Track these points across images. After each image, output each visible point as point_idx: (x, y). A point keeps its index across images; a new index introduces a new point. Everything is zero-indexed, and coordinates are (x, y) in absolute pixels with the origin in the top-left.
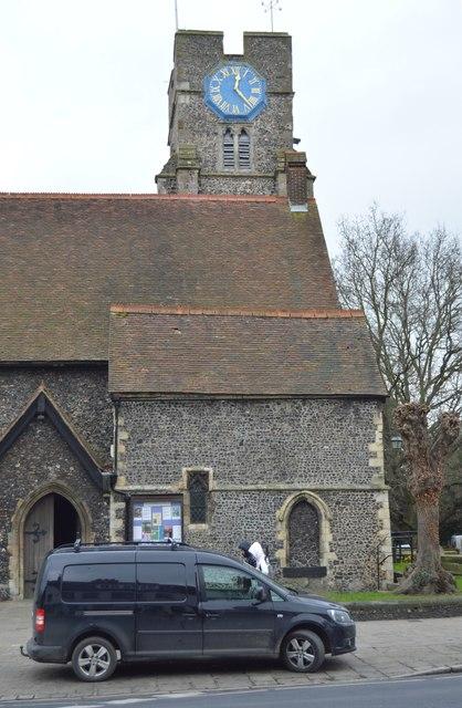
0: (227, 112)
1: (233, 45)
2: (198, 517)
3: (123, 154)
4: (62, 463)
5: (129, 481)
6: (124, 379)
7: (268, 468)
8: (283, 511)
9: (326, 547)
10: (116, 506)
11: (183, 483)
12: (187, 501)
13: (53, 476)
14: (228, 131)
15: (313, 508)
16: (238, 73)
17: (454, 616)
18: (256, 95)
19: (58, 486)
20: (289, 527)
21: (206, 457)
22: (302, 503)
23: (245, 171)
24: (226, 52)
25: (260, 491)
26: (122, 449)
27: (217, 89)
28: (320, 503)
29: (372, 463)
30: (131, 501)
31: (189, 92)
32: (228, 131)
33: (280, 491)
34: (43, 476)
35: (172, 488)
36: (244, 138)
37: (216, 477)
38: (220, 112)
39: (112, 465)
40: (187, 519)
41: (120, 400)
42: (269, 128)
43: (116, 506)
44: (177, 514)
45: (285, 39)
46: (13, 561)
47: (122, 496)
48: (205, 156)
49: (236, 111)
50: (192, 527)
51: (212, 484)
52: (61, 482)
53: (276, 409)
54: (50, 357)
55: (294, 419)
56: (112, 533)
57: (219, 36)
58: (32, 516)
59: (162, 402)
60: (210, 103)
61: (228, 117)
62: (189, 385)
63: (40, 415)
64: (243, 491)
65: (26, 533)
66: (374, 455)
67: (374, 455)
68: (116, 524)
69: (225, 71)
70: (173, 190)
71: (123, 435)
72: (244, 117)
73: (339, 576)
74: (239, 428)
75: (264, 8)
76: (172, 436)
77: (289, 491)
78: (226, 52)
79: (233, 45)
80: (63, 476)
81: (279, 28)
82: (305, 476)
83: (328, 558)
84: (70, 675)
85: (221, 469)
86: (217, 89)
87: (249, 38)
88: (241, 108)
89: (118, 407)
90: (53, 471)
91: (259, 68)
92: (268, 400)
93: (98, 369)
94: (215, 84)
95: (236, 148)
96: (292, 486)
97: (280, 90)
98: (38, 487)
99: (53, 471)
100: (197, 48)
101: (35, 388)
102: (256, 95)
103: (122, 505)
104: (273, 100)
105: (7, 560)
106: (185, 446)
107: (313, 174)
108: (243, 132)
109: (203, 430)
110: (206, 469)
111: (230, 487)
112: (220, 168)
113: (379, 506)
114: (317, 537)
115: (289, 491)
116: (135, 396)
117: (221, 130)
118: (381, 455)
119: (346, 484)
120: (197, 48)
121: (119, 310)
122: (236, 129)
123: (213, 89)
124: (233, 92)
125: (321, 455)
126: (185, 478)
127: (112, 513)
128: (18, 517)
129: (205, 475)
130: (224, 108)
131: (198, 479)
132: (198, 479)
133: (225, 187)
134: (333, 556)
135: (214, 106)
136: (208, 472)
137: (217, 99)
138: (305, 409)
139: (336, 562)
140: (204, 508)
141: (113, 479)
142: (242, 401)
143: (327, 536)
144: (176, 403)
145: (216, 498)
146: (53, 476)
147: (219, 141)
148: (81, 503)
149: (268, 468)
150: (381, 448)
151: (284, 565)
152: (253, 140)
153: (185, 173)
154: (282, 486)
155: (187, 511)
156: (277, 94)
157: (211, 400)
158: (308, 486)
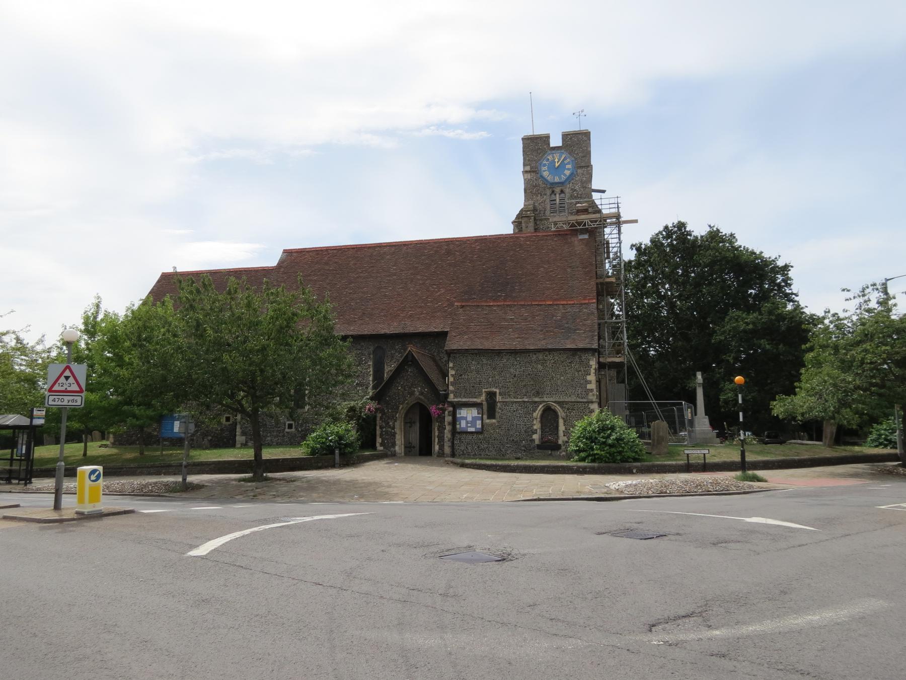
0: (552, 181)
1: (556, 141)
2: (491, 415)
3: (489, 208)
5: (455, 396)
6: (452, 344)
8: (537, 414)
11: (483, 397)
12: (485, 407)
13: (417, 393)
14: (553, 192)
15: (555, 413)
16: (557, 159)
18: (568, 169)
20: (541, 422)
24: (552, 145)
26: (451, 379)
27: (546, 168)
28: (558, 408)
29: (589, 387)
30: (456, 406)
32: (553, 192)
33: (536, 402)
34: (412, 393)
35: (478, 400)
36: (562, 195)
39: (447, 390)
40: (485, 417)
41: (450, 353)
46: (398, 437)
48: (539, 207)
49: (557, 180)
50: (488, 421)
51: (499, 398)
56: (446, 423)
60: (542, 176)
61: (553, 185)
63: (409, 361)
64: (516, 402)
65: (406, 423)
66: (590, 382)
67: (590, 382)
68: (448, 419)
69: (550, 157)
71: (452, 372)
72: (562, 183)
76: (478, 372)
77: (541, 403)
78: (552, 145)
79: (556, 141)
80: (421, 393)
82: (550, 394)
86: (546, 168)
87: (566, 136)
88: (560, 178)
89: (449, 356)
91: (571, 153)
94: (545, 165)
98: (411, 401)
100: (535, 147)
102: (568, 169)
103: (451, 409)
104: (579, 171)
105: (394, 436)
108: (562, 192)
109: (494, 369)
113: (381, 445)
115: (541, 403)
116: (458, 351)
117: (548, 192)
118: (594, 382)
119: (573, 399)
120: (535, 147)
122: (558, 190)
123: (544, 168)
125: (559, 382)
126: (484, 395)
129: (495, 393)
130: (550, 179)
131: (491, 396)
132: (491, 396)
137: (546, 174)
138: (550, 357)
141: (446, 396)
146: (417, 393)
148: (433, 409)
150: (237, 438)
152: (568, 195)
153: (526, 219)
154: (537, 399)
156: (581, 167)
157: (499, 353)
158: (551, 399)
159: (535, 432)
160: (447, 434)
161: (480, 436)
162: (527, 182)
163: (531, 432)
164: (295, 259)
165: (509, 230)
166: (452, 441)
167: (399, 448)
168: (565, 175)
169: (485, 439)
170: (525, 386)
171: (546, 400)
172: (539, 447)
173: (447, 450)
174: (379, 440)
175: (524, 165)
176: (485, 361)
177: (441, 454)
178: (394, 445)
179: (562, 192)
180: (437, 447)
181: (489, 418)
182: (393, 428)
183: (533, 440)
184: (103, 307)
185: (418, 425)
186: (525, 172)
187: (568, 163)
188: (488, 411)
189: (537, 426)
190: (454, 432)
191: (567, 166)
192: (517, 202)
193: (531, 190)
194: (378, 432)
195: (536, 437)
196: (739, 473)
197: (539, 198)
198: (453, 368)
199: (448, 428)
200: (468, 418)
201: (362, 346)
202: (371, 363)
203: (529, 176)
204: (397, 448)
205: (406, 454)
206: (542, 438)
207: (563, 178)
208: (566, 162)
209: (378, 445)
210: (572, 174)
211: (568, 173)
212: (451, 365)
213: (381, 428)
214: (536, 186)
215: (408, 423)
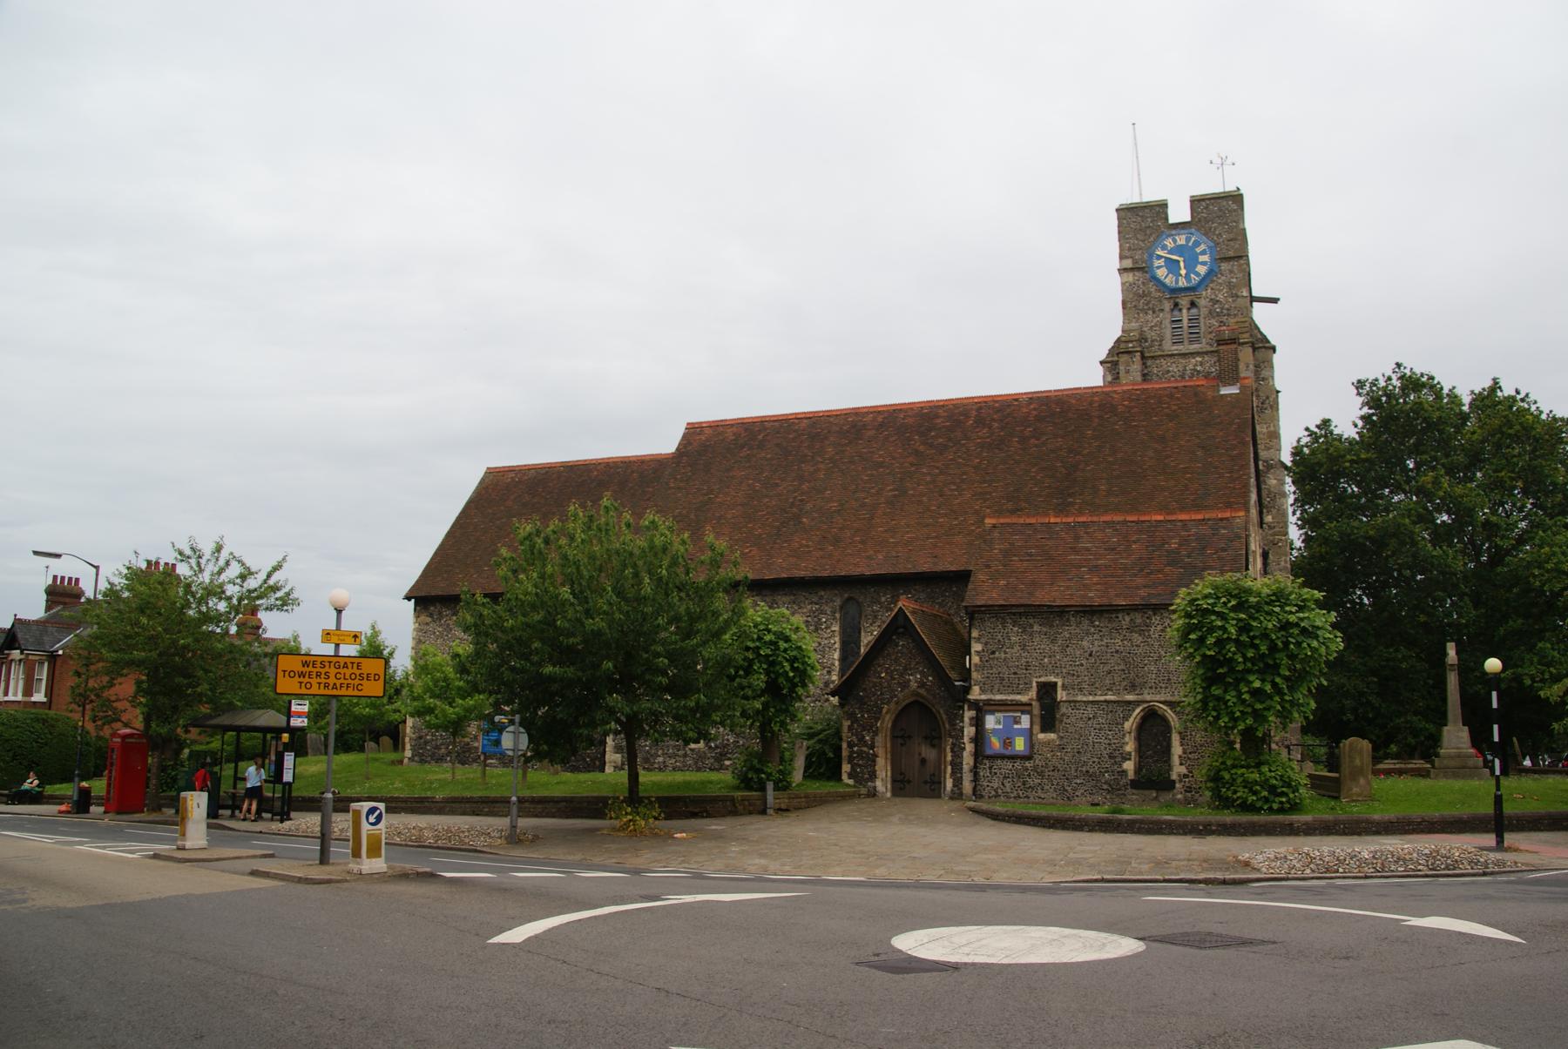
1: (1179, 212)
2: (1048, 723)
4: (922, 673)
5: (983, 691)
6: (984, 591)
7: (1117, 679)
9: (1176, 760)
10: (969, 714)
11: (1033, 693)
13: (914, 685)
14: (1176, 305)
15: (1164, 720)
17: (1487, 832)
18: (1204, 263)
19: (918, 694)
20: (1139, 739)
23: (1195, 347)
24: (1172, 220)
26: (976, 659)
27: (1162, 262)
28: (1170, 714)
30: (981, 709)
31: (1132, 269)
32: (1176, 305)
33: (1129, 702)
35: (1024, 698)
36: (1194, 311)
37: (1064, 687)
38: (1164, 285)
39: (966, 675)
40: (1037, 728)
41: (974, 613)
42: (1220, 297)
43: (969, 714)
45: (1236, 199)
46: (881, 762)
48: (1151, 335)
50: (1041, 736)
51: (1061, 695)
52: (922, 691)
53: (1126, 620)
55: (1143, 630)
56: (966, 740)
57: (1162, 206)
61: (1176, 291)
62: (1042, 597)
65: (894, 737)
70: (1117, 377)
73: (1189, 790)
74: (1089, 641)
75: (1214, 167)
77: (1138, 703)
78: (1172, 220)
79: (1179, 212)
80: (922, 685)
81: (1230, 188)
82: (1156, 688)
83: (1178, 770)
85: (1068, 680)
87: (1196, 202)
90: (914, 680)
92: (1118, 611)
95: (1185, 321)
96: (1140, 698)
97: (1231, 254)
98: (903, 697)
99: (914, 680)
100: (1141, 223)
101: (895, 600)
102: (1204, 263)
103: (973, 713)
104: (1225, 266)
106: (1038, 656)
107: (1056, 335)
108: (1193, 304)
109: (1053, 641)
110: (1052, 679)
111: (1079, 698)
112: (1168, 347)
115: (1138, 703)
117: (1167, 306)
120: (1141, 223)
121: (993, 521)
122: (1184, 302)
124: (1189, 262)
127: (966, 719)
128: (886, 722)
130: (1169, 281)
131: (1047, 690)
132: (1047, 690)
133: (1174, 368)
134: (1183, 770)
136: (1055, 684)
137: (1161, 273)
138: (1156, 620)
139: (1185, 776)
140: (1053, 718)
141: (967, 690)
142: (1091, 612)
143: (1177, 750)
144: (1026, 614)
146: (914, 685)
147: (1166, 318)
149: (1117, 679)
151: (1131, 775)
152: (1204, 311)
154: (1130, 697)
155: (1037, 720)
157: (1055, 614)
158: (1158, 698)
159: (1126, 757)
160: (968, 759)
162: (1126, 289)
163: (1118, 756)
165: (1091, 376)
166: (975, 771)
167: (882, 784)
168: (1198, 274)
169: (1035, 768)
171: (1148, 698)
172: (1135, 784)
173: (967, 786)
174: (846, 768)
175: (1122, 257)
176: (1036, 628)
177: (957, 795)
178: (873, 776)
179: (1193, 304)
180: (949, 784)
181: (1043, 730)
182: (872, 747)
183: (1124, 772)
186: (1122, 271)
187: (1203, 253)
188: (1042, 717)
189: (1130, 747)
190: (978, 755)
192: (1109, 325)
193: (1134, 303)
194: (845, 753)
195: (1129, 766)
196: (1489, 839)
197: (1149, 317)
198: (978, 640)
199: (969, 747)
200: (1009, 730)
201: (821, 597)
202: (836, 628)
203: (1130, 277)
204: (879, 783)
206: (1138, 770)
207: (1195, 279)
208: (1198, 250)
209: (845, 777)
210: (1210, 272)
211: (1202, 270)
212: (975, 634)
213: (850, 745)
214: (1144, 295)
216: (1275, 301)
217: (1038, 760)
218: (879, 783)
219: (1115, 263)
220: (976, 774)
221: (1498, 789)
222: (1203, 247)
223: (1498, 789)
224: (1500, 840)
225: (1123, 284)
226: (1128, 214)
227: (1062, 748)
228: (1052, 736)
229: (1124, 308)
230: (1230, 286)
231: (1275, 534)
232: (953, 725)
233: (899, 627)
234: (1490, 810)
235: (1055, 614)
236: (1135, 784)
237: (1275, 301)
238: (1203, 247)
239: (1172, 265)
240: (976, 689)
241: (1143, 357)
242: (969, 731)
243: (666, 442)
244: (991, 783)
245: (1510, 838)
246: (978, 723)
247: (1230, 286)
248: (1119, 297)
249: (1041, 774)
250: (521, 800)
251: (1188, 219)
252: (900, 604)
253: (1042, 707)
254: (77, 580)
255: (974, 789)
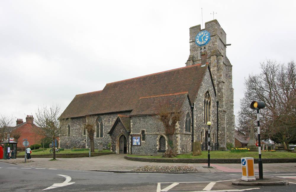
1: (203, 27)
2: (144, 139)
6: (132, 114)
9: (166, 146)
10: (130, 137)
11: (141, 133)
12: (141, 136)
13: (122, 132)
14: (201, 48)
15: (164, 137)
18: (207, 38)
20: (160, 142)
21: (145, 127)
22: (162, 137)
25: (154, 134)
26: (131, 126)
27: (198, 39)
31: (192, 42)
32: (201, 48)
33: (157, 134)
34: (120, 132)
35: (139, 134)
36: (205, 49)
37: (146, 131)
40: (142, 140)
42: (211, 45)
43: (130, 137)
44: (190, 131)
47: (131, 135)
48: (195, 56)
50: (142, 141)
51: (146, 133)
54: (111, 111)
57: (200, 26)
58: (122, 137)
59: (138, 117)
60: (197, 43)
61: (201, 45)
78: (201, 29)
79: (203, 27)
80: (123, 131)
84: (170, 156)
86: (198, 39)
93: (130, 111)
97: (213, 35)
100: (195, 30)
102: (207, 38)
104: (212, 38)
107: (174, 56)
108: (205, 48)
109: (145, 122)
111: (149, 133)
114: (165, 144)
117: (199, 49)
120: (195, 30)
122: (203, 48)
128: (118, 138)
129: (144, 131)
130: (200, 43)
131: (143, 132)
132: (143, 132)
135: (197, 43)
137: (198, 42)
141: (130, 132)
144: (140, 117)
145: (146, 136)
146: (122, 132)
149: (156, 129)
151: (158, 149)
152: (207, 49)
154: (158, 133)
160: (130, 146)
161: (140, 147)
162: (191, 46)
164: (110, 87)
165: (184, 66)
167: (117, 151)
168: (206, 41)
169: (141, 148)
170: (154, 128)
172: (158, 151)
175: (190, 39)
179: (205, 48)
181: (143, 140)
183: (157, 149)
184: (251, 76)
185: (123, 142)
189: (158, 143)
190: (132, 145)
191: (206, 37)
192: (186, 54)
193: (192, 49)
195: (158, 147)
196: (207, 165)
198: (132, 122)
199: (130, 144)
203: (192, 44)
205: (120, 153)
206: (160, 148)
210: (209, 40)
211: (206, 40)
212: (131, 121)
215: (120, 142)
216: (230, 45)
217: (142, 146)
218: (116, 151)
219: (189, 41)
220: (131, 149)
221: (209, 153)
222: (207, 34)
223: (209, 153)
224: (209, 165)
225: (190, 45)
226: (192, 29)
227: (146, 144)
228: (144, 141)
229: (190, 51)
230: (213, 42)
231: (220, 98)
232: (128, 139)
233: (118, 121)
234: (207, 158)
235: (145, 116)
236: (158, 151)
237: (230, 45)
238: (207, 34)
239: (201, 40)
240: (132, 132)
241: (193, 61)
242: (130, 141)
243: (100, 87)
244: (134, 151)
245: (211, 165)
246: (132, 139)
247: (213, 42)
248: (189, 48)
249: (142, 149)
250: (209, 155)
251: (204, 28)
252: (118, 116)
253: (143, 136)
254: (22, 119)
255: (131, 152)
